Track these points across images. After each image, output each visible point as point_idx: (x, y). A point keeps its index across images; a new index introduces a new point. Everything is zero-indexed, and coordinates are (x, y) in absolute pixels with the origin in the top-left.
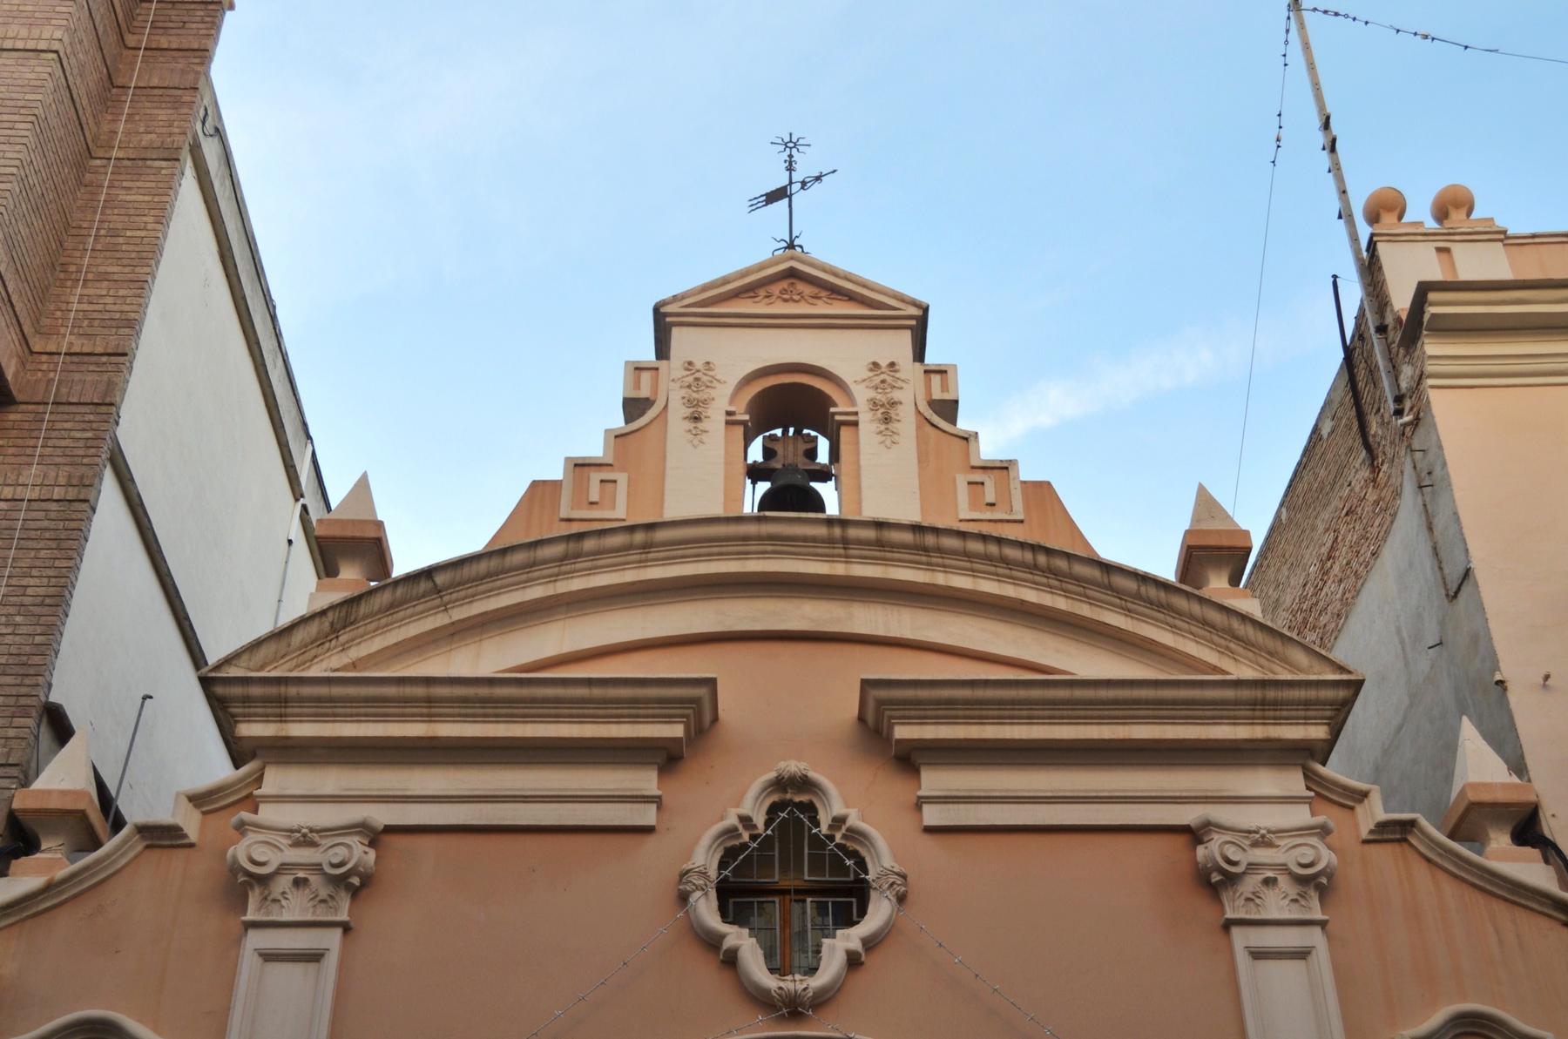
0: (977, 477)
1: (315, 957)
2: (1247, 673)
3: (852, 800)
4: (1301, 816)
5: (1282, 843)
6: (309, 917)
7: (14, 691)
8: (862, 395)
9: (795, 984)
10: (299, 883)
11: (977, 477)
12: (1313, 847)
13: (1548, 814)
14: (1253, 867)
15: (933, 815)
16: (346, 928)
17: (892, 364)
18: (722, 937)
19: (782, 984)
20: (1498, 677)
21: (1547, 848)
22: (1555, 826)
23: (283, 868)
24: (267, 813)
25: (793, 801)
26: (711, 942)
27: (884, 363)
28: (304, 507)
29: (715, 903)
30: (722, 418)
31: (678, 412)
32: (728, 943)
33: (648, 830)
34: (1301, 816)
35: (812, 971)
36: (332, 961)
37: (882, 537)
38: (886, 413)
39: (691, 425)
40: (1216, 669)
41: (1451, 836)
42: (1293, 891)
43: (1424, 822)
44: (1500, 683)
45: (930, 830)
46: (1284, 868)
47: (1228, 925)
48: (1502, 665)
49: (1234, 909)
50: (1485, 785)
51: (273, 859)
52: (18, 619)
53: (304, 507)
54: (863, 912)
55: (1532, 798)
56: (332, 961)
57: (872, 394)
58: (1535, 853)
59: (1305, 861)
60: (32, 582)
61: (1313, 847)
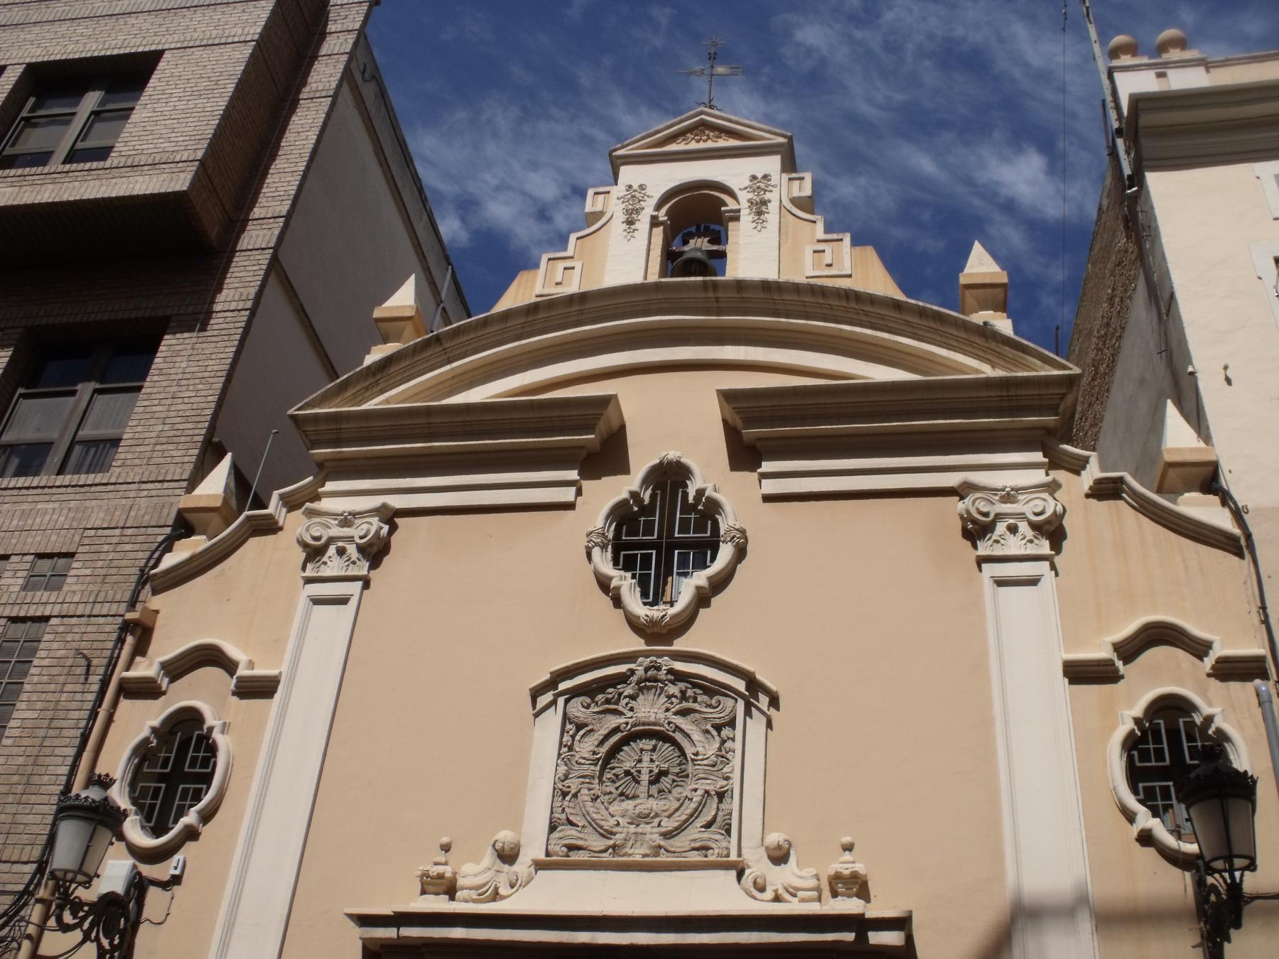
0: (820, 247)
1: (343, 601)
2: (988, 371)
3: (710, 473)
4: (1039, 476)
5: (1021, 497)
6: (343, 573)
7: (191, 432)
8: (744, 197)
9: (655, 612)
10: (1013, 529)
11: (820, 247)
12: (1044, 500)
13: (1226, 473)
14: (999, 517)
15: (771, 487)
16: (367, 584)
17: (765, 177)
18: (611, 578)
19: (649, 613)
20: (1190, 369)
21: (1226, 499)
22: (1228, 480)
23: (331, 540)
24: (326, 504)
25: (669, 477)
26: (604, 584)
27: (760, 176)
28: (444, 309)
29: (609, 555)
30: (648, 220)
31: (620, 216)
32: (614, 584)
33: (570, 506)
34: (1039, 476)
35: (672, 604)
36: (353, 603)
37: (770, 295)
38: (759, 208)
39: (625, 226)
40: (977, 371)
41: (1159, 491)
42: (1030, 534)
43: (1129, 479)
44: (1192, 374)
45: (768, 499)
46: (1021, 516)
47: (981, 561)
48: (1194, 361)
49: (984, 548)
50: (1178, 450)
51: (326, 533)
52: (200, 387)
53: (444, 309)
54: (713, 559)
55: (1213, 458)
56: (353, 603)
57: (751, 196)
58: (1215, 499)
59: (1038, 510)
60: (211, 362)
61: (1044, 500)
